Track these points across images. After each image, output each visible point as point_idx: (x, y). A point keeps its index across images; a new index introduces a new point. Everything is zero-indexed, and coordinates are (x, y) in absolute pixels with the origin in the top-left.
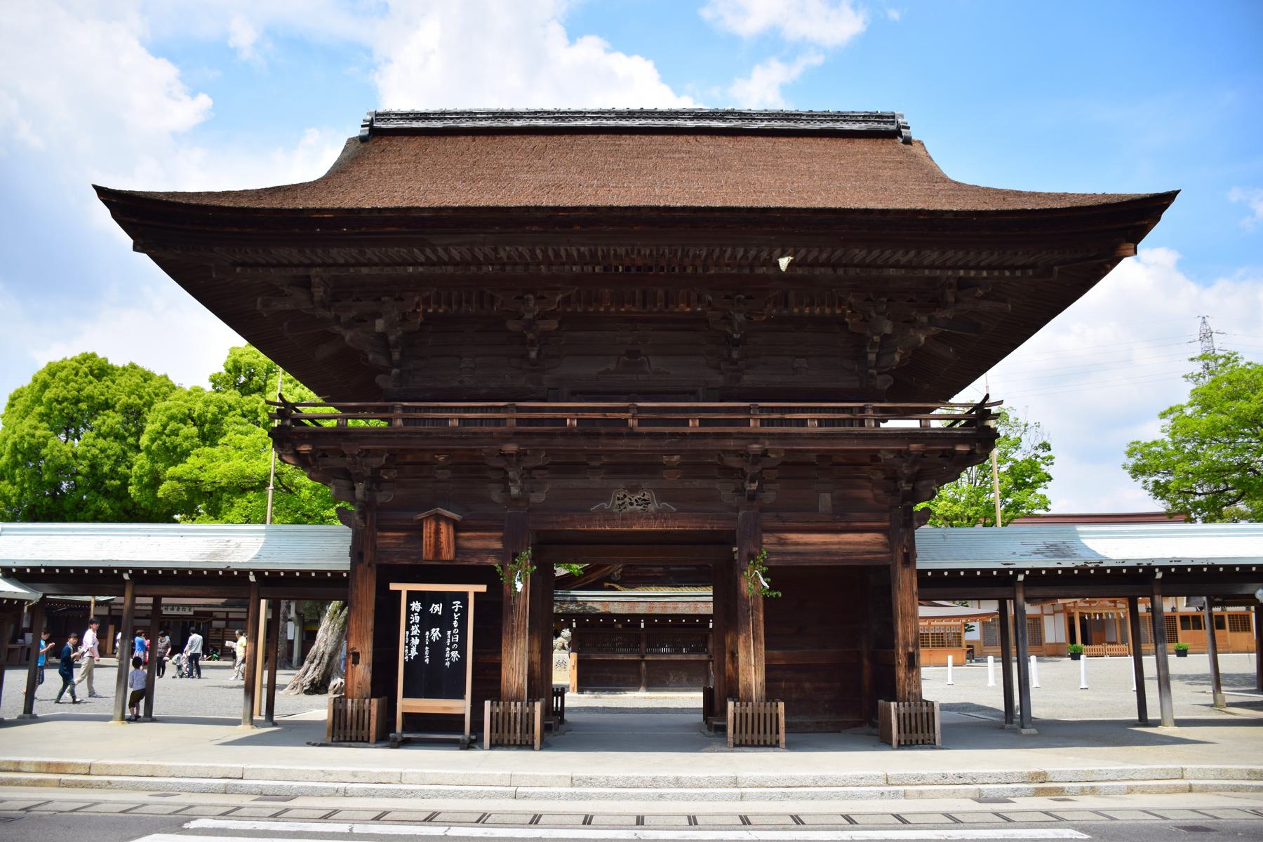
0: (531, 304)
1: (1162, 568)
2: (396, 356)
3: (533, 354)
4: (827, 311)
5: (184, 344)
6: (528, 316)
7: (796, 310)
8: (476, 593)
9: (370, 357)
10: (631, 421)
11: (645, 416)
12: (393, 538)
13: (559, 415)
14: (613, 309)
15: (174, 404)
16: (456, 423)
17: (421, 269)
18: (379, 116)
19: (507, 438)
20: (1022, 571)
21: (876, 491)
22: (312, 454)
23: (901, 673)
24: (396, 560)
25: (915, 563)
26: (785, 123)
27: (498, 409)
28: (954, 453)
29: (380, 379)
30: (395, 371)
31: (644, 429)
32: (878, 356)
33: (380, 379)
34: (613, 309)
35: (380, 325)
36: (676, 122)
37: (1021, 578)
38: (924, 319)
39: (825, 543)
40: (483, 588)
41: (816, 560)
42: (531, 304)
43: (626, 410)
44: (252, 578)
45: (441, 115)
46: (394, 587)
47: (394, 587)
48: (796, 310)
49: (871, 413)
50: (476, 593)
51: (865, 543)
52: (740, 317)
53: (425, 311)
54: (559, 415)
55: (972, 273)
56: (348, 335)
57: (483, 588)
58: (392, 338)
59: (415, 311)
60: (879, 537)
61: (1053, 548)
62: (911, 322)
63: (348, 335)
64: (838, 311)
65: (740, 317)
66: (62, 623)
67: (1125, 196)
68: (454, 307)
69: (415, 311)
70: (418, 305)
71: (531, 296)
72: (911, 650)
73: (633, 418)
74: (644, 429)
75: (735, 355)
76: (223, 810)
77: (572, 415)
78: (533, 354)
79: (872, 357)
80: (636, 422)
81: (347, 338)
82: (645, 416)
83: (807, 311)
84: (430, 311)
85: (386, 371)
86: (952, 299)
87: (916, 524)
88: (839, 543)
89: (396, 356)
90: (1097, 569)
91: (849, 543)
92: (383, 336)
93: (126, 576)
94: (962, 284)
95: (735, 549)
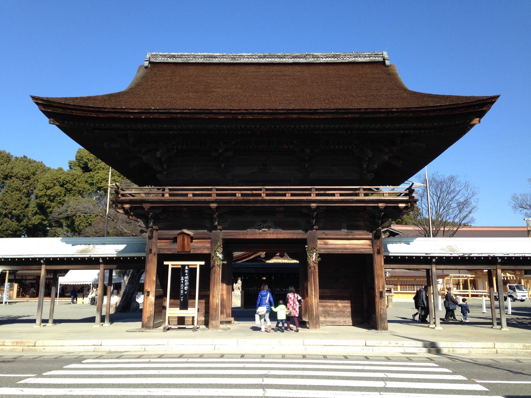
1: (500, 257)
2: (165, 166)
3: (223, 166)
5: (58, 152)
6: (221, 151)
7: (332, 147)
8: (200, 266)
9: (154, 167)
10: (262, 195)
11: (268, 192)
12: (164, 242)
13: (233, 192)
15: (44, 178)
16: (191, 195)
17: (176, 132)
19: (213, 202)
22: (130, 208)
23: (377, 299)
24: (166, 252)
26: (333, 59)
27: (208, 190)
30: (165, 173)
31: (268, 198)
35: (158, 154)
36: (284, 59)
37: (434, 260)
38: (387, 150)
39: (344, 244)
40: (203, 263)
41: (340, 252)
43: (261, 190)
44: (101, 261)
46: (165, 263)
47: (165, 263)
50: (200, 266)
51: (361, 245)
52: (308, 151)
54: (233, 192)
55: (407, 132)
56: (144, 158)
57: (203, 263)
58: (163, 159)
60: (368, 242)
61: (450, 248)
63: (144, 158)
64: (350, 147)
65: (308, 151)
67: (473, 97)
72: (381, 290)
73: (263, 193)
74: (268, 198)
75: (306, 165)
76: (96, 357)
77: (239, 192)
78: (223, 166)
79: (365, 166)
80: (265, 195)
82: (268, 192)
88: (350, 244)
89: (165, 166)
90: (469, 257)
91: (355, 245)
93: (42, 261)
95: (306, 246)
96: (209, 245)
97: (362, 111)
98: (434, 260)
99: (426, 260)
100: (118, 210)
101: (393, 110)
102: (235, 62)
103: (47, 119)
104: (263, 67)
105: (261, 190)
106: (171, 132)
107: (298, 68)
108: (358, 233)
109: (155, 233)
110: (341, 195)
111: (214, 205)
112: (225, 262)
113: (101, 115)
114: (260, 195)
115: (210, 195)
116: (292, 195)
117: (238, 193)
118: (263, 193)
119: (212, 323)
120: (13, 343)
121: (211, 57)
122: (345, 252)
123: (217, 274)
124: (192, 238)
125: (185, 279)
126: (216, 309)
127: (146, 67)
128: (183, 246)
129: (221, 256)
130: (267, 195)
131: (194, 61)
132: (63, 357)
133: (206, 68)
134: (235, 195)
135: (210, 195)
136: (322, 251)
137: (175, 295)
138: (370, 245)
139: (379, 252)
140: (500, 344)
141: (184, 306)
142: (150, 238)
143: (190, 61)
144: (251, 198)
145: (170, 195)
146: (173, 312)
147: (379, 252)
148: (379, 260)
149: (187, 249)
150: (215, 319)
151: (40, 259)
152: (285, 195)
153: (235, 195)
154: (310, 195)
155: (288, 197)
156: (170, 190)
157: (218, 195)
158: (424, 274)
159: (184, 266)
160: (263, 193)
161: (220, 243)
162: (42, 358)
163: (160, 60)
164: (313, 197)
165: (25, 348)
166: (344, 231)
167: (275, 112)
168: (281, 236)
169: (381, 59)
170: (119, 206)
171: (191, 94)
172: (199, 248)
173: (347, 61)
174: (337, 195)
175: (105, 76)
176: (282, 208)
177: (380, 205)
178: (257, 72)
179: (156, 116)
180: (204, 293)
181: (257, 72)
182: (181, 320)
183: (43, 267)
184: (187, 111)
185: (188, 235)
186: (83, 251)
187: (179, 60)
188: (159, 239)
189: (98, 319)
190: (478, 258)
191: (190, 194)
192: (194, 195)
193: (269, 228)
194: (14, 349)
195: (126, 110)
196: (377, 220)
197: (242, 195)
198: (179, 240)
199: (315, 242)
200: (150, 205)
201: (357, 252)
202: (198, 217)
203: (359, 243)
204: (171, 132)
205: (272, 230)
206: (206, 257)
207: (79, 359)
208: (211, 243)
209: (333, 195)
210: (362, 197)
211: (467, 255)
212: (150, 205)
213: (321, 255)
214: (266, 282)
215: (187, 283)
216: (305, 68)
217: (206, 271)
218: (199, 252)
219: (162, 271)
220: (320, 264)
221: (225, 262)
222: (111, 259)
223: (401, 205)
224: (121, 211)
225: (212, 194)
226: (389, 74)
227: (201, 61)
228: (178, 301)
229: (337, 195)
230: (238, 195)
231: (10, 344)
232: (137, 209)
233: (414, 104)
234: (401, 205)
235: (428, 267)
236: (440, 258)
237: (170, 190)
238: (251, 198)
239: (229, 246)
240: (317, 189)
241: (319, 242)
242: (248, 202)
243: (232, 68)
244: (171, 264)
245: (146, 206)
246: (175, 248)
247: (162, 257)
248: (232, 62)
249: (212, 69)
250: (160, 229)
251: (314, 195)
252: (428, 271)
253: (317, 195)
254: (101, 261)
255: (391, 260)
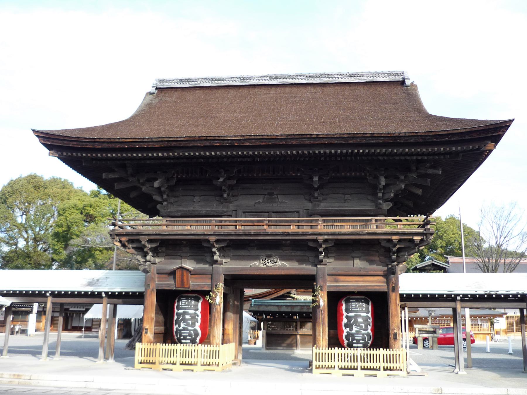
0: (223, 174)
3: (225, 195)
4: (358, 174)
9: (154, 197)
14: (260, 175)
17: (172, 161)
18: (161, 81)
20: (459, 295)
21: (381, 258)
25: (398, 291)
28: (412, 241)
29: (158, 206)
30: (165, 203)
32: (383, 193)
33: (158, 206)
34: (260, 175)
35: (156, 184)
37: (458, 298)
38: (402, 177)
42: (223, 174)
44: (104, 295)
45: (188, 80)
48: (343, 174)
49: (374, 222)
53: (177, 177)
55: (431, 157)
58: (163, 189)
59: (172, 177)
62: (397, 178)
64: (363, 174)
66: (18, 312)
67: (497, 121)
68: (190, 175)
69: (172, 177)
70: (174, 174)
71: (222, 170)
75: (316, 194)
78: (225, 195)
81: (143, 189)
83: (348, 174)
84: (179, 176)
85: (161, 203)
86: (414, 168)
87: (399, 273)
92: (159, 188)
94: (418, 162)
97: (368, 135)
98: (458, 298)
99: (450, 298)
100: (115, 243)
101: (401, 135)
102: (244, 84)
103: (47, 151)
104: (273, 89)
106: (168, 161)
120: (10, 375)
132: (52, 392)
133: (214, 91)
138: (384, 282)
140: (513, 390)
143: (197, 86)
151: (46, 292)
158: (450, 312)
162: (33, 391)
165: (20, 380)
169: (400, 78)
170: (117, 238)
173: (365, 81)
175: (109, 103)
176: (288, 242)
184: (182, 139)
189: (45, 351)
194: (11, 381)
195: (121, 141)
196: (388, 253)
198: (178, 274)
200: (217, 238)
204: (168, 161)
211: (494, 293)
212: (217, 238)
216: (319, 89)
226: (409, 94)
231: (8, 376)
232: (134, 240)
233: (443, 128)
235: (452, 304)
236: (465, 296)
237: (376, 220)
248: (241, 84)
251: (323, 228)
252: (455, 310)
254: (104, 295)
255: (406, 298)
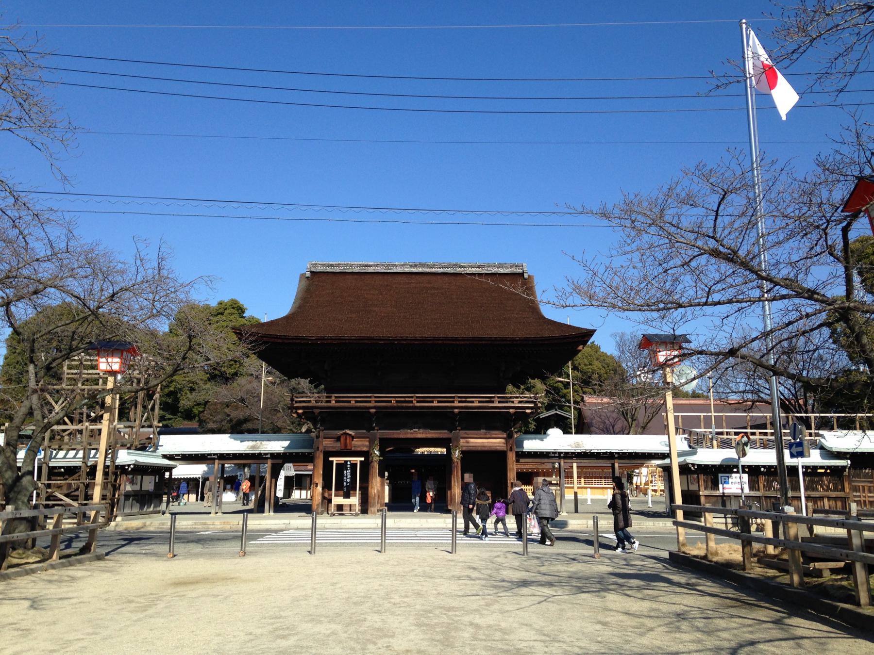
19: (372, 408)
40: (363, 459)
41: (479, 449)
43: (412, 397)
46: (331, 459)
47: (331, 459)
57: (363, 459)
60: (503, 440)
96: (367, 443)
105: (412, 397)
107: (446, 278)
108: (495, 433)
109: (321, 433)
110: (480, 402)
111: (373, 411)
112: (589, 502)
113: (286, 341)
114: (411, 402)
115: (370, 402)
116: (439, 402)
117: (393, 399)
118: (415, 400)
119: (372, 509)
121: (367, 266)
122: (484, 449)
123: (375, 468)
124: (353, 438)
125: (348, 473)
126: (374, 498)
127: (308, 278)
128: (346, 445)
129: (377, 453)
130: (418, 402)
131: (351, 270)
134: (390, 402)
135: (370, 402)
136: (464, 449)
137: (339, 487)
139: (511, 449)
141: (347, 496)
142: (318, 437)
144: (404, 405)
145: (336, 402)
146: (337, 500)
147: (511, 449)
148: (511, 457)
149: (349, 447)
150: (373, 506)
152: (432, 402)
153: (390, 402)
154: (453, 402)
155: (435, 404)
156: (336, 397)
157: (376, 402)
159: (346, 462)
160: (415, 400)
161: (377, 442)
163: (320, 269)
164: (456, 404)
166: (483, 431)
167: (424, 339)
168: (429, 436)
169: (520, 271)
171: (354, 315)
172: (359, 446)
174: (476, 401)
177: (511, 410)
178: (409, 283)
179: (330, 341)
180: (364, 485)
181: (409, 283)
182: (340, 508)
183: (217, 461)
185: (350, 435)
186: (253, 447)
187: (337, 270)
188: (325, 438)
190: (599, 453)
191: (354, 400)
192: (356, 402)
193: (419, 428)
197: (397, 402)
199: (458, 441)
201: (493, 449)
202: (359, 419)
203: (495, 442)
205: (421, 431)
206: (366, 454)
207: (276, 531)
208: (370, 442)
209: (473, 402)
210: (496, 404)
213: (463, 452)
214: (414, 485)
215: (349, 476)
216: (453, 278)
217: (366, 466)
218: (359, 449)
219: (328, 466)
220: (462, 460)
221: (589, 502)
222: (278, 454)
223: (528, 411)
224: (295, 415)
225: (371, 401)
227: (357, 270)
228: (342, 492)
229: (476, 401)
230: (393, 401)
232: (309, 414)
234: (528, 411)
238: (404, 405)
239: (384, 443)
240: (459, 397)
241: (462, 440)
242: (402, 407)
243: (386, 277)
244: (335, 460)
245: (317, 411)
246: (338, 446)
247: (328, 454)
249: (367, 277)
250: (325, 429)
251: (457, 402)
253: (460, 402)
